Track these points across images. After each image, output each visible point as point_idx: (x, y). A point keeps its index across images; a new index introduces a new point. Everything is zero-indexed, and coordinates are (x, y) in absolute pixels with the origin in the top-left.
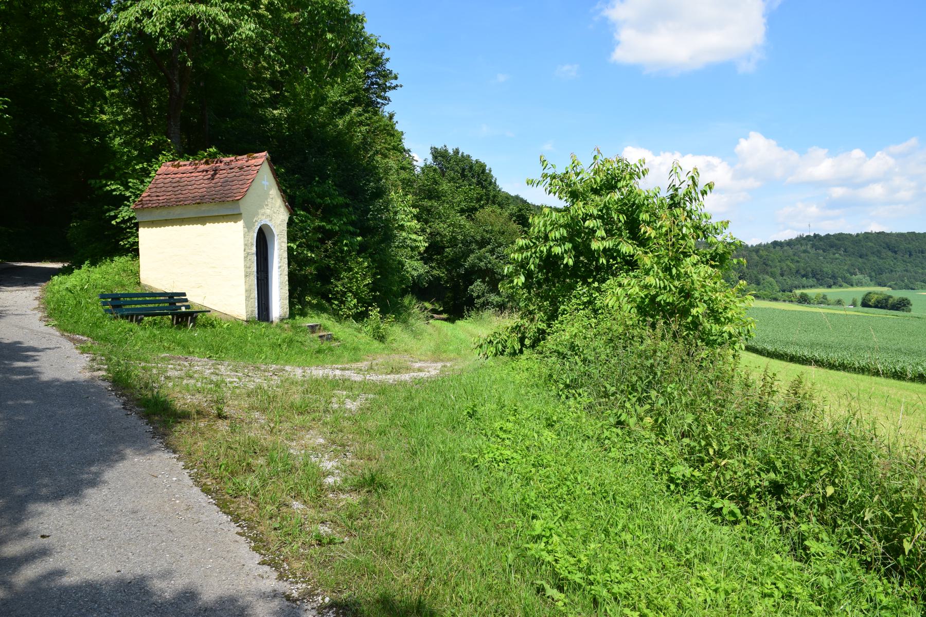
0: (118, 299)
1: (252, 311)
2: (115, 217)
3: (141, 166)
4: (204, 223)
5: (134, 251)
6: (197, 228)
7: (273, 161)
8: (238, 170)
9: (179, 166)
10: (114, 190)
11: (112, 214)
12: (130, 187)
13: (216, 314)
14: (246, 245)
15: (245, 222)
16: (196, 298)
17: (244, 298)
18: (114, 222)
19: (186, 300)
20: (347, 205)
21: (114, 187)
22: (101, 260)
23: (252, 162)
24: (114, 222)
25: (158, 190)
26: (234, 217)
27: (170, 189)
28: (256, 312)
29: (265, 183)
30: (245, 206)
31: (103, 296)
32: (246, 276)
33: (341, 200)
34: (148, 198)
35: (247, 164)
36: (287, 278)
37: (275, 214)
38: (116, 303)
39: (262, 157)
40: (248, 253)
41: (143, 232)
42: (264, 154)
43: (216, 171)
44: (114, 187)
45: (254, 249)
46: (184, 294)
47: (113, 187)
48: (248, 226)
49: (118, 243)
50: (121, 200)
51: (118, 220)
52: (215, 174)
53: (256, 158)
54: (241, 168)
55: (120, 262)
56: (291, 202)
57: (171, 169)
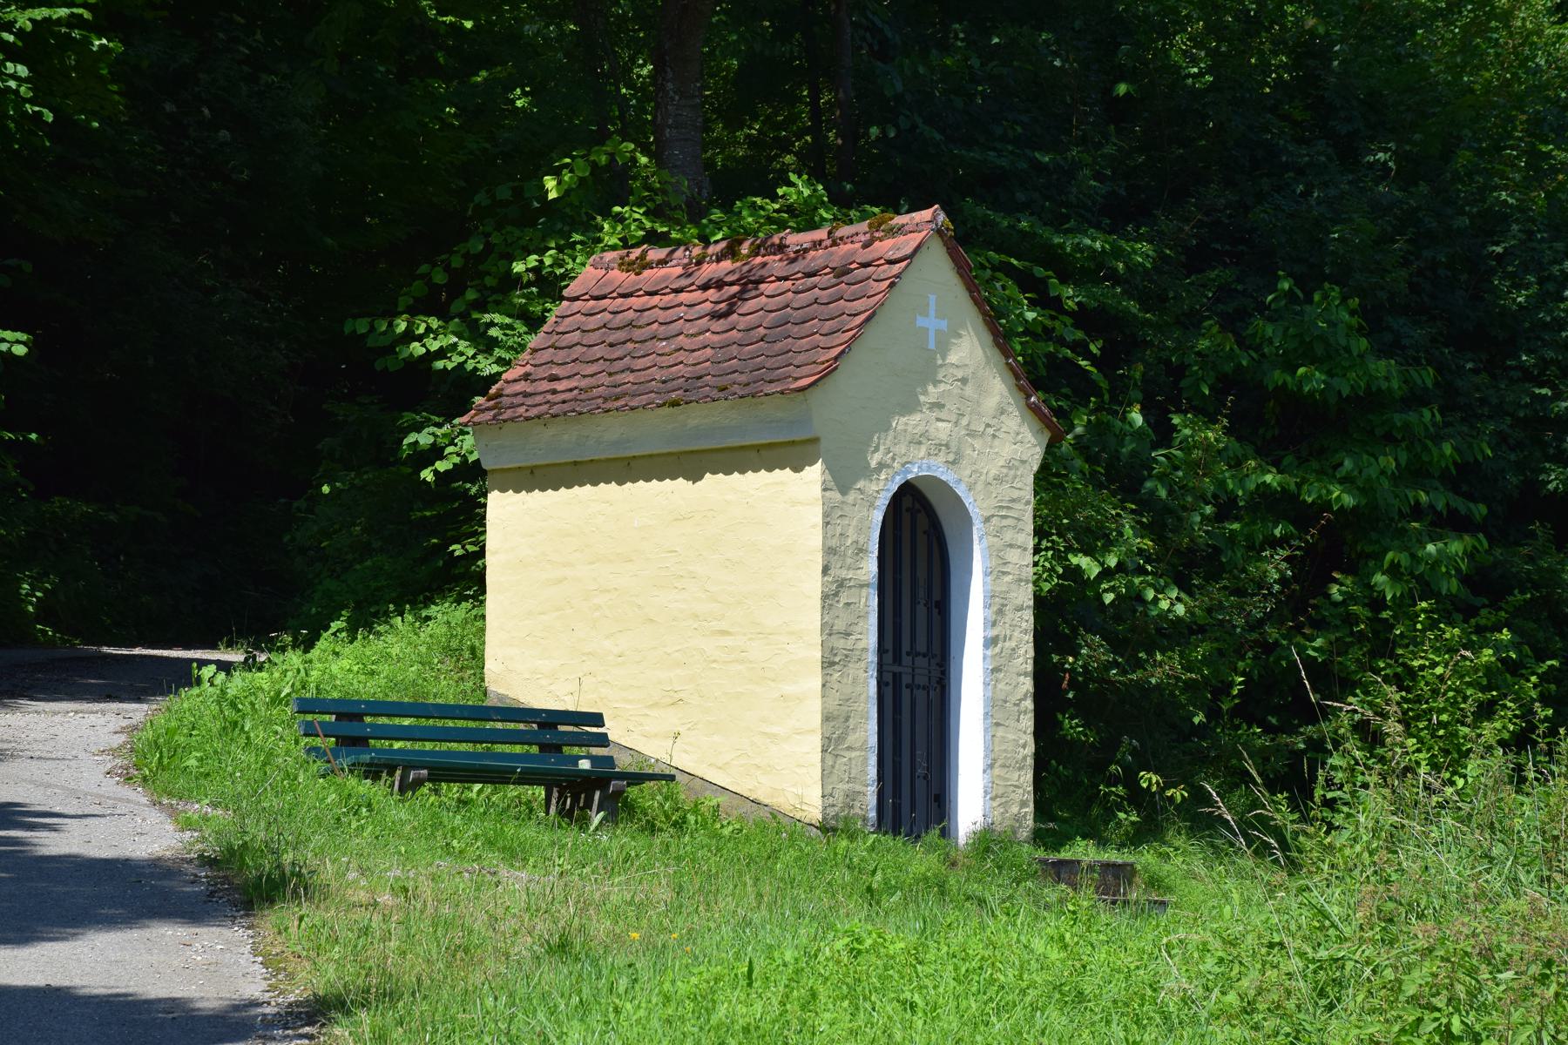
0: (358, 717)
1: (852, 796)
2: (436, 452)
3: (532, 260)
4: (695, 477)
5: (466, 580)
6: (608, 491)
7: (963, 240)
8: (828, 279)
9: (643, 265)
10: (442, 353)
11: (424, 439)
12: (495, 342)
13: (721, 799)
14: (829, 551)
15: (830, 468)
16: (637, 734)
17: (816, 741)
18: (427, 475)
19: (603, 740)
20: (1415, 399)
21: (435, 341)
22: (385, 617)
23: (886, 247)
24: (427, 475)
25: (561, 356)
26: (787, 453)
27: (598, 351)
28: (871, 799)
29: (931, 323)
30: (830, 410)
31: (305, 706)
32: (828, 664)
33: (1384, 371)
34: (519, 387)
35: (866, 255)
36: (1028, 684)
37: (981, 439)
38: (351, 729)
39: (922, 223)
40: (841, 584)
41: (504, 511)
42: (926, 214)
43: (749, 284)
44: (435, 341)
45: (871, 567)
46: (597, 719)
47: (434, 346)
48: (842, 479)
49: (435, 558)
50: (457, 393)
51: (442, 466)
52: (740, 297)
53: (899, 230)
54: (842, 272)
55: (445, 615)
56: (1044, 379)
57: (617, 275)
